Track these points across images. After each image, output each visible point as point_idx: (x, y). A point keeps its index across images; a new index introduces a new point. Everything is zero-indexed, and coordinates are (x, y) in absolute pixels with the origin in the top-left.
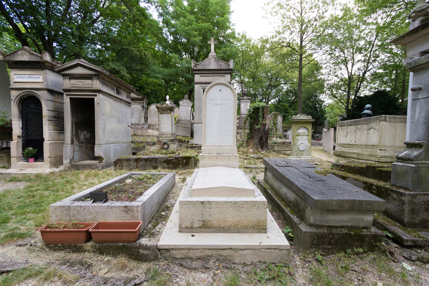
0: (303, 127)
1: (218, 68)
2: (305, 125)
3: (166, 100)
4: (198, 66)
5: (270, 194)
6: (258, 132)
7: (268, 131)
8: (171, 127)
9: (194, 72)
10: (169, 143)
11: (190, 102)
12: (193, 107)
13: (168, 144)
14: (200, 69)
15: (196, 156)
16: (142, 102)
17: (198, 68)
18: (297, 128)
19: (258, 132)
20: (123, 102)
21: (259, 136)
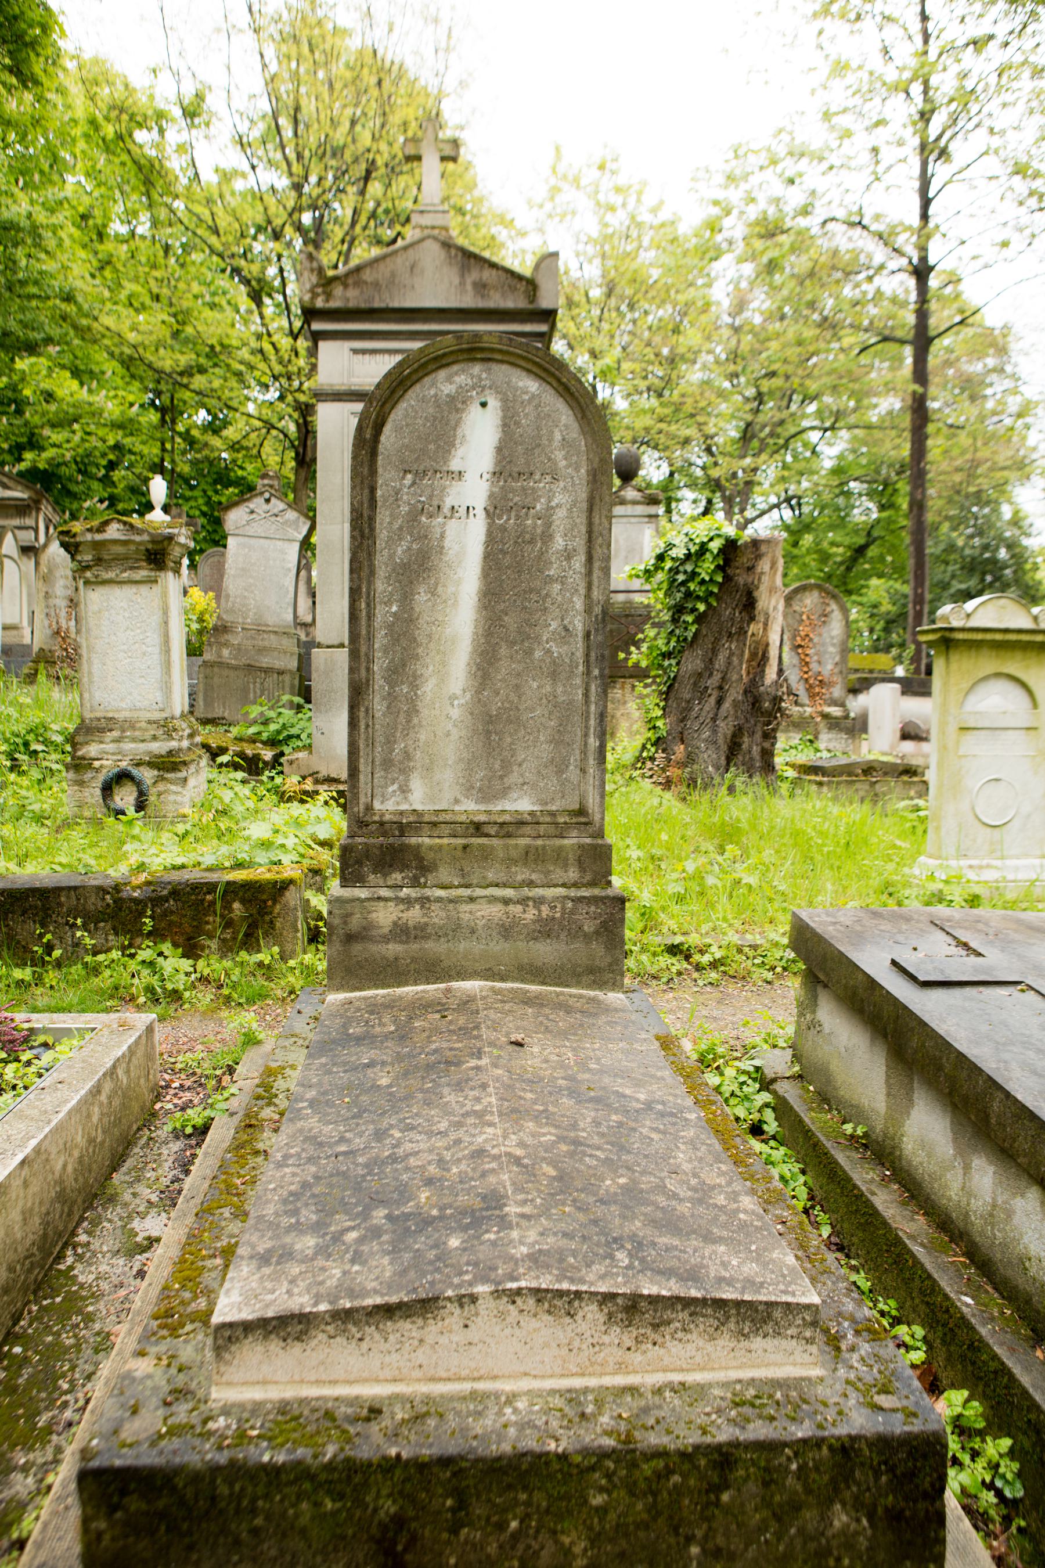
0: (998, 675)
1: (469, 301)
2: (1013, 666)
3: (149, 507)
4: (338, 290)
5: (964, 1322)
6: (719, 702)
7: (777, 700)
8: (157, 672)
9: (316, 326)
10: (147, 775)
11: (292, 515)
12: (306, 545)
13: (138, 784)
14: (351, 305)
15: (559, 190)
16: (29, 522)
17: (334, 304)
18: (966, 685)
19: (719, 702)
20: (985, 651)
21: (725, 728)
